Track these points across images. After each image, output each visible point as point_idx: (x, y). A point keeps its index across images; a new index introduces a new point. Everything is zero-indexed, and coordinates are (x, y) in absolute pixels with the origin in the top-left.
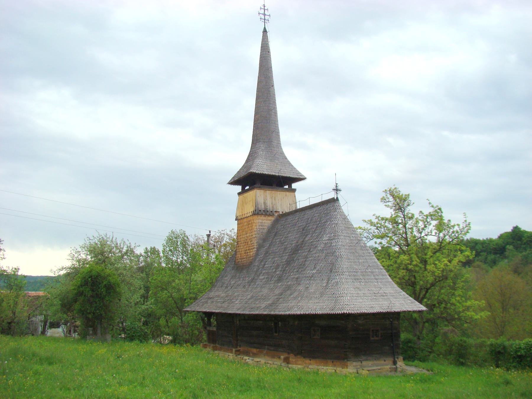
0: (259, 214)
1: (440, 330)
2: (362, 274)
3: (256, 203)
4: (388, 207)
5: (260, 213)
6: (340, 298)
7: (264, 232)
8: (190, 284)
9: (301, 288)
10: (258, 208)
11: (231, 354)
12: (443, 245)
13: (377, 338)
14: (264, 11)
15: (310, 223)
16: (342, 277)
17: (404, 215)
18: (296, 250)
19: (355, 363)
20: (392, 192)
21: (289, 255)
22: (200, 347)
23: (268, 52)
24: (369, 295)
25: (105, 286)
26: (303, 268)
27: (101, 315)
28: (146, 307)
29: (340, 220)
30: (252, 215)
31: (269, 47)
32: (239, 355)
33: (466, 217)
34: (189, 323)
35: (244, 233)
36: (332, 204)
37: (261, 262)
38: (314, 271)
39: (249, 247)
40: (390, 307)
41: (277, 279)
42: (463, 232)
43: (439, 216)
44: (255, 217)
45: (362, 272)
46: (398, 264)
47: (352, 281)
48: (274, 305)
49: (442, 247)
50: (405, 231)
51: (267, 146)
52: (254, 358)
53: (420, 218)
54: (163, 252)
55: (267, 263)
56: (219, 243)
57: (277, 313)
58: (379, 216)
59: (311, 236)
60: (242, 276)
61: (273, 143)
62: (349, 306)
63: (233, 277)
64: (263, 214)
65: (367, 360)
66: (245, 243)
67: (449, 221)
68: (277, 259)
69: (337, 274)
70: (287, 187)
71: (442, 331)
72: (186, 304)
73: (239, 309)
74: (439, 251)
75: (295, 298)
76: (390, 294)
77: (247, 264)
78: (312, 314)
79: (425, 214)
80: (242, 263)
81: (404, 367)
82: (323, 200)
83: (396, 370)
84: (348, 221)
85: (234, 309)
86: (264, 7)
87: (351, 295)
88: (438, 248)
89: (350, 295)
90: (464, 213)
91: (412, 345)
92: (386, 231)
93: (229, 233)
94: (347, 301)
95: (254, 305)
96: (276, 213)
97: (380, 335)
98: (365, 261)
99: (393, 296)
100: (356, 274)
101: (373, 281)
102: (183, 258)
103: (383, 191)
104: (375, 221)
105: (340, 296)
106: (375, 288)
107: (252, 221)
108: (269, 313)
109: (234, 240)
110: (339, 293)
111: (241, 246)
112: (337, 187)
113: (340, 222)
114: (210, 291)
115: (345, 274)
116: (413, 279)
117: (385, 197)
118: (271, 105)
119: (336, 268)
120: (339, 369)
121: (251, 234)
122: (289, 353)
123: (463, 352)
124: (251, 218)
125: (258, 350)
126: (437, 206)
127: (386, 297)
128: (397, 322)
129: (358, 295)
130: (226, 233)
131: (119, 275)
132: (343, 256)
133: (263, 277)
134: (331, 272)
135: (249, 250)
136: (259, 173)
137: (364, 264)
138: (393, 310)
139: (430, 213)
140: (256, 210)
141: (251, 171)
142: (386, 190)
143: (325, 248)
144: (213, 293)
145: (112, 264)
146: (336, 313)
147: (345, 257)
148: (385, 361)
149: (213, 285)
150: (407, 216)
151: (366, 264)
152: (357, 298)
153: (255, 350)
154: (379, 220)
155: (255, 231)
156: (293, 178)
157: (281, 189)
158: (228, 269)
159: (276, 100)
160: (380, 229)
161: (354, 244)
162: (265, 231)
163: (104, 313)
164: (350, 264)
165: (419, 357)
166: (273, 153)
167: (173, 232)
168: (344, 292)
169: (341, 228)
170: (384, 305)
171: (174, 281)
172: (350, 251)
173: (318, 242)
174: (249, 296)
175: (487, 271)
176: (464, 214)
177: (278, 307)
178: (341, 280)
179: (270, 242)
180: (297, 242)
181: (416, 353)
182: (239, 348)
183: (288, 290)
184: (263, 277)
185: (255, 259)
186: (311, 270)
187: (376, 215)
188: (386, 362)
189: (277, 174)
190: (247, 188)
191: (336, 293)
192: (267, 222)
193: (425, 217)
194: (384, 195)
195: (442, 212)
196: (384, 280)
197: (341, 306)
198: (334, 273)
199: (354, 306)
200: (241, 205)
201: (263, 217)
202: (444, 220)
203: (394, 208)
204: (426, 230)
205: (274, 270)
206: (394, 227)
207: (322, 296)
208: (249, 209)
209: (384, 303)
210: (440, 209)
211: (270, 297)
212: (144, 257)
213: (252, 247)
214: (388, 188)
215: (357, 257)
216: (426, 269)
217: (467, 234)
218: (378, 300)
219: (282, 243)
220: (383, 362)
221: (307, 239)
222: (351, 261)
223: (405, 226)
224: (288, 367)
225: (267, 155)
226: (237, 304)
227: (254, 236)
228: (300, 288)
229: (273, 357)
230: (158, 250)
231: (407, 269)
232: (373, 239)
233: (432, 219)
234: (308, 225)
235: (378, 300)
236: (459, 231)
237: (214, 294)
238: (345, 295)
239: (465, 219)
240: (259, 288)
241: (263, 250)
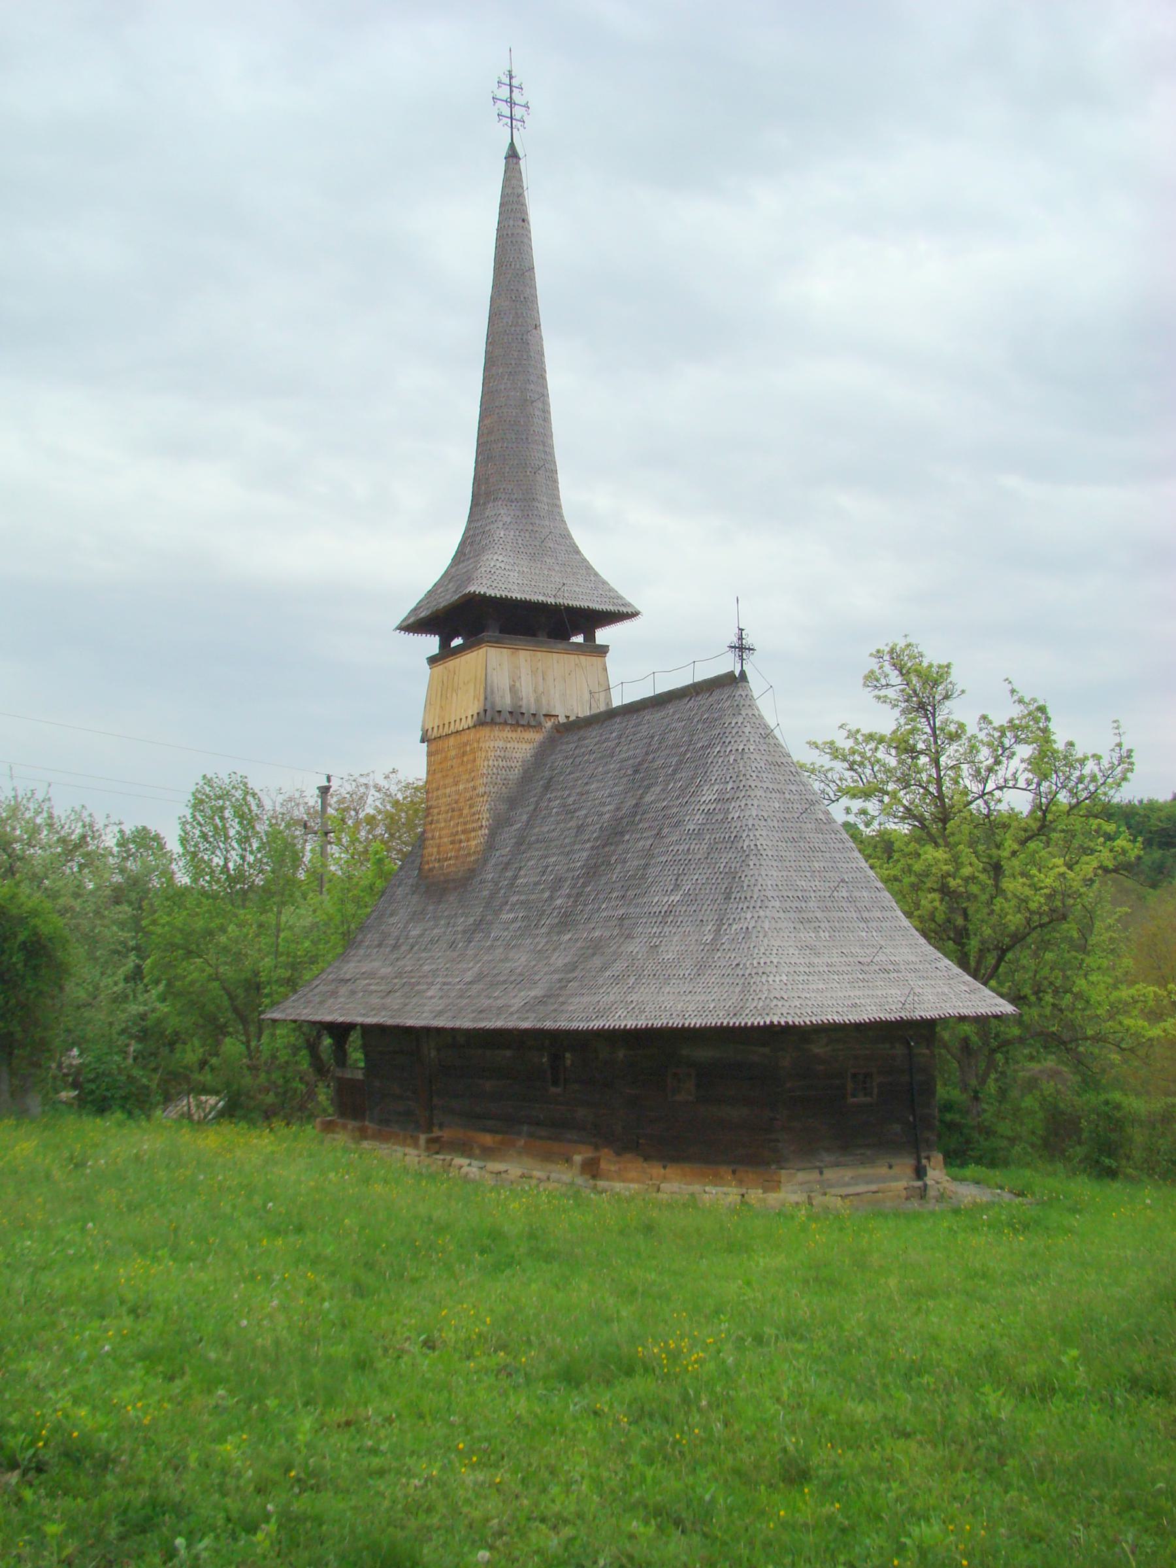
0: (496, 724)
1: (1015, 1071)
2: (821, 904)
3: (486, 688)
4: (885, 702)
5: (498, 720)
6: (759, 979)
7: (511, 777)
8: (278, 937)
9: (637, 949)
10: (493, 704)
11: (411, 1151)
12: (1049, 817)
13: (868, 1099)
14: (511, 92)
15: (658, 749)
16: (762, 913)
17: (933, 729)
18: (615, 833)
19: (801, 1176)
20: (898, 656)
21: (592, 848)
22: (311, 1130)
23: (523, 221)
24: (845, 969)
26: (639, 886)
28: (142, 1009)
30: (475, 726)
31: (524, 205)
32: (437, 1153)
34: (274, 1057)
35: (450, 780)
36: (727, 691)
37: (505, 869)
39: (465, 823)
40: (907, 1006)
41: (556, 921)
42: (1110, 780)
43: (1039, 728)
44: (485, 732)
45: (822, 899)
46: (917, 875)
47: (792, 925)
48: (552, 1000)
49: (1047, 823)
50: (935, 776)
51: (519, 513)
52: (484, 1160)
53: (982, 736)
54: (184, 841)
55: (522, 873)
56: (353, 813)
57: (563, 1024)
58: (858, 731)
59: (663, 790)
60: (446, 914)
61: (537, 504)
62: (785, 1003)
63: (417, 916)
64: (510, 722)
65: (837, 1165)
66: (453, 810)
67: (1071, 744)
68: (554, 859)
69: (747, 904)
70: (579, 639)
71: (1021, 1074)
72: (267, 1001)
73: (440, 1014)
74: (1039, 835)
75: (617, 979)
76: (908, 967)
77: (460, 874)
78: (671, 1028)
79: (996, 724)
80: (444, 874)
81: (947, 1185)
82: (699, 678)
83: (923, 1193)
84: (777, 745)
85: (425, 1015)
86: (511, 78)
87: (792, 970)
88: (1035, 826)
89: (787, 969)
90: (1115, 722)
91: (957, 1117)
92: (879, 775)
93: (383, 783)
94: (778, 988)
95: (487, 1002)
97: (876, 1091)
98: (830, 865)
99: (916, 970)
100: (804, 905)
101: (856, 925)
102: (243, 858)
103: (871, 655)
104: (846, 744)
105: (757, 973)
106: (862, 947)
107: (475, 745)
108: (539, 1025)
109: (396, 803)
110: (755, 962)
111: (438, 821)
112: (741, 638)
113: (752, 748)
114: (343, 957)
115: (770, 905)
116: (960, 921)
117: (878, 672)
118: (532, 387)
119: (742, 887)
120: (755, 1195)
121: (472, 784)
122: (597, 1148)
123: (1114, 1136)
124: (472, 735)
125: (499, 1137)
126: (1034, 700)
127: (895, 975)
128: (927, 1051)
129: (812, 969)
130: (371, 783)
131: (62, 913)
132: (762, 852)
133: (512, 916)
134: (728, 898)
135: (464, 832)
136: (496, 597)
137: (826, 874)
138: (917, 1015)
139: (1011, 721)
140: (485, 711)
141: (472, 589)
142: (878, 651)
143: (708, 826)
144: (352, 965)
145: (36, 879)
146: (746, 1024)
147: (770, 853)
148: (890, 1167)
149: (350, 941)
150: (942, 730)
151: (832, 874)
152: (810, 978)
153: (488, 1139)
154: (857, 742)
155: (483, 775)
156: (599, 611)
157: (561, 645)
158: (400, 891)
159: (547, 369)
160: (860, 770)
161: (797, 815)
162: (515, 774)
163: (19, 1029)
164: (784, 874)
165: (976, 1154)
166: (537, 535)
167: (209, 782)
168: (768, 961)
169: (756, 764)
170: (890, 1000)
171: (223, 929)
172: (786, 835)
173: (686, 808)
174: (470, 973)
175: (1141, 898)
176: (1115, 725)
177: (564, 1007)
178: (760, 923)
179: (532, 808)
180: (618, 809)
181: (968, 1142)
182: (437, 1133)
183: (594, 954)
184: (512, 916)
185: (485, 861)
186: (665, 893)
187: (848, 728)
190: (457, 642)
191: (745, 964)
193: (997, 734)
194: (873, 664)
195: (1048, 719)
196: (888, 924)
197: (761, 1003)
198: (738, 903)
199: (800, 1001)
200: (439, 695)
201: (507, 733)
202: (1055, 742)
203: (903, 705)
204: (1000, 774)
205: (546, 895)
206: (901, 762)
207: (700, 972)
208: (466, 708)
209: (890, 992)
210: (1042, 709)
211: (537, 977)
212: (118, 857)
213: (475, 825)
214: (887, 645)
215: (806, 854)
216: (999, 891)
217: (1123, 784)
218: (871, 984)
219: (570, 812)
220: (884, 1170)
221: (648, 798)
222: (788, 864)
223: (936, 762)
224: (594, 1188)
225: (520, 542)
226: (431, 998)
227: (481, 790)
228: (634, 947)
229: (547, 1157)
230: (157, 835)
231: (944, 890)
232: (837, 800)
233: (1018, 740)
234: (651, 757)
235: (871, 984)
236: (1099, 775)
237: (356, 967)
238: (775, 970)
239: (1117, 740)
240: (501, 950)
241: (508, 836)
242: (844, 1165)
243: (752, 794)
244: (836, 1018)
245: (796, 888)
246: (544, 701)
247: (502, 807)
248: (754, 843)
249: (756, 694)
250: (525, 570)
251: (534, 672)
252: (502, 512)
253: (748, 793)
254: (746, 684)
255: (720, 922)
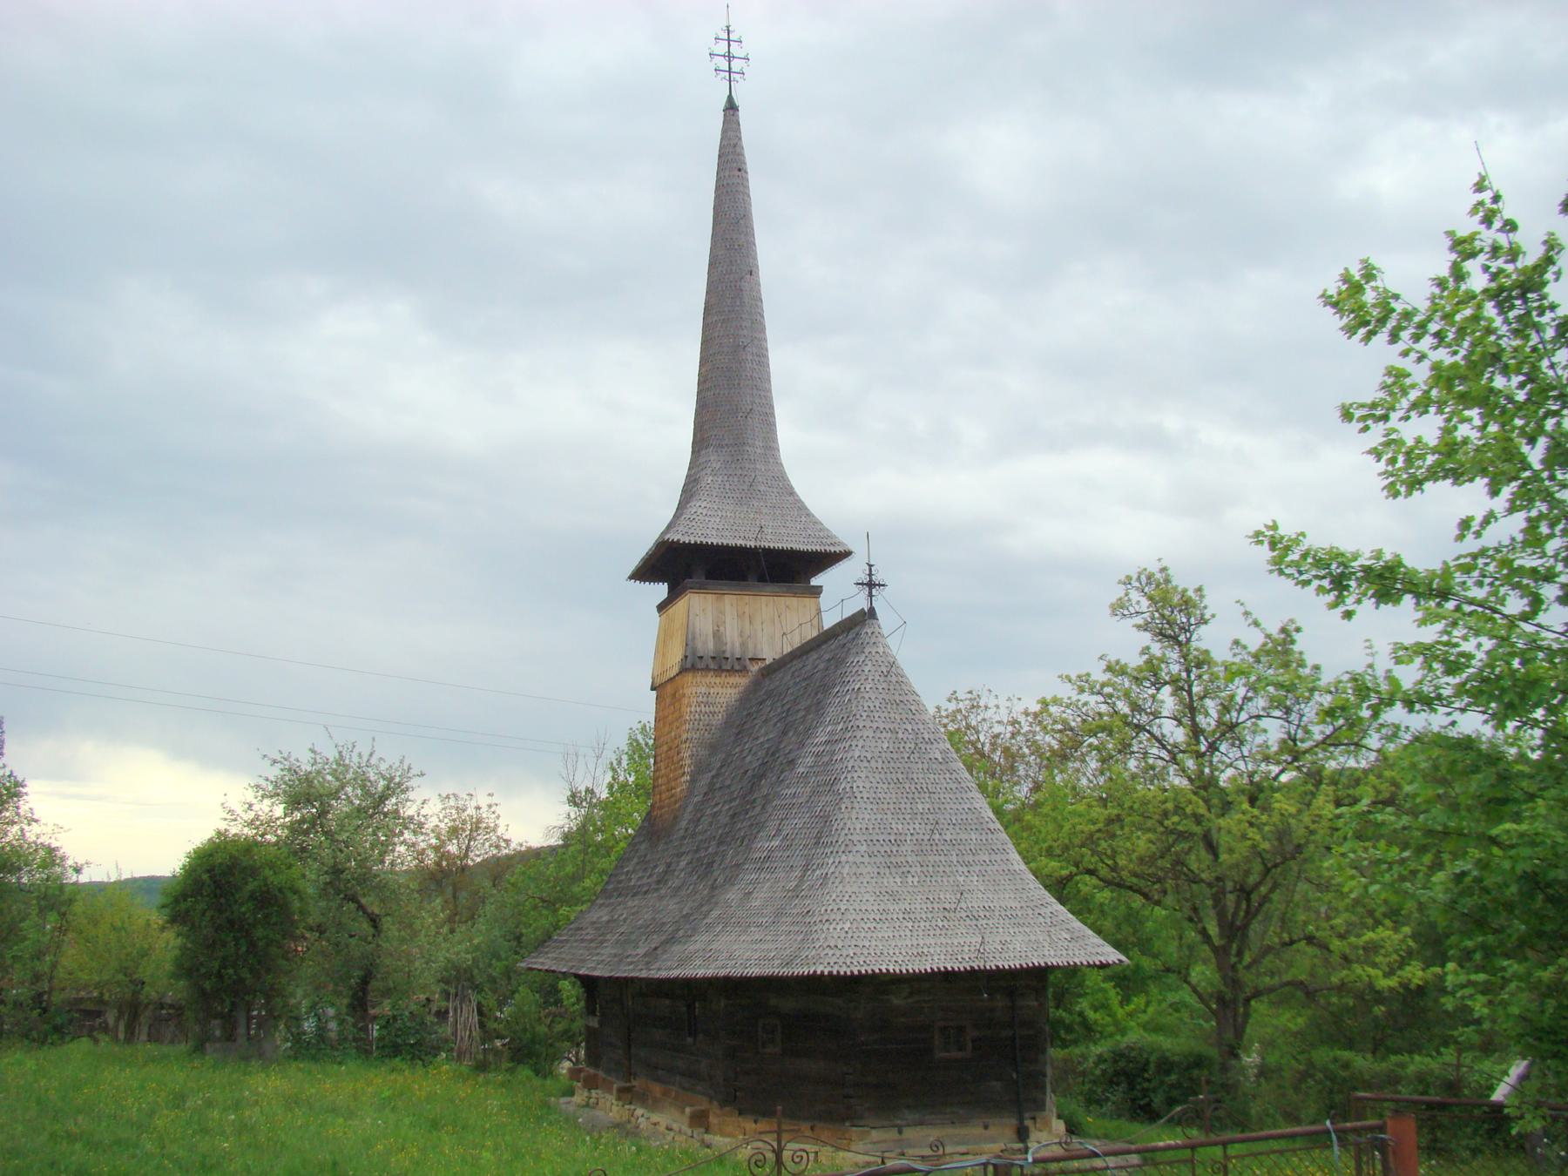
0: (723, 671)
10: (694, 653)
16: (844, 858)
25: (252, 896)
27: (241, 980)
29: (870, 678)
33: (1373, 655)
38: (775, 843)
44: (689, 678)
47: (876, 870)
65: (921, 1124)
69: (831, 849)
78: (746, 977)
89: (854, 917)
96: (754, 663)
97: (970, 1045)
104: (1099, 676)
112: (870, 575)
113: (868, 687)
115: (855, 849)
118: (745, 332)
128: (1036, 1003)
132: (857, 794)
136: (690, 543)
138: (991, 965)
147: (865, 796)
148: (986, 1127)
152: (878, 926)
153: (657, 1089)
162: (718, 720)
164: (879, 816)
176: (1367, 644)
188: (992, 1131)
189: (752, 544)
191: (814, 912)
192: (725, 692)
194: (1119, 592)
197: (814, 952)
201: (711, 679)
220: (978, 1131)
225: (727, 487)
239: (1369, 660)
242: (931, 1124)
243: (859, 734)
244: (973, 965)
245: (890, 831)
246: (751, 646)
247: (703, 753)
248: (850, 785)
249: (885, 632)
250: (729, 514)
251: (740, 616)
252: (712, 458)
253: (855, 734)
254: (874, 621)
255: (806, 868)
